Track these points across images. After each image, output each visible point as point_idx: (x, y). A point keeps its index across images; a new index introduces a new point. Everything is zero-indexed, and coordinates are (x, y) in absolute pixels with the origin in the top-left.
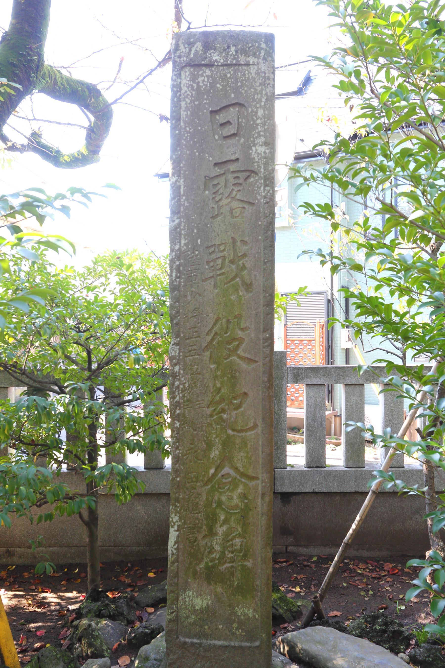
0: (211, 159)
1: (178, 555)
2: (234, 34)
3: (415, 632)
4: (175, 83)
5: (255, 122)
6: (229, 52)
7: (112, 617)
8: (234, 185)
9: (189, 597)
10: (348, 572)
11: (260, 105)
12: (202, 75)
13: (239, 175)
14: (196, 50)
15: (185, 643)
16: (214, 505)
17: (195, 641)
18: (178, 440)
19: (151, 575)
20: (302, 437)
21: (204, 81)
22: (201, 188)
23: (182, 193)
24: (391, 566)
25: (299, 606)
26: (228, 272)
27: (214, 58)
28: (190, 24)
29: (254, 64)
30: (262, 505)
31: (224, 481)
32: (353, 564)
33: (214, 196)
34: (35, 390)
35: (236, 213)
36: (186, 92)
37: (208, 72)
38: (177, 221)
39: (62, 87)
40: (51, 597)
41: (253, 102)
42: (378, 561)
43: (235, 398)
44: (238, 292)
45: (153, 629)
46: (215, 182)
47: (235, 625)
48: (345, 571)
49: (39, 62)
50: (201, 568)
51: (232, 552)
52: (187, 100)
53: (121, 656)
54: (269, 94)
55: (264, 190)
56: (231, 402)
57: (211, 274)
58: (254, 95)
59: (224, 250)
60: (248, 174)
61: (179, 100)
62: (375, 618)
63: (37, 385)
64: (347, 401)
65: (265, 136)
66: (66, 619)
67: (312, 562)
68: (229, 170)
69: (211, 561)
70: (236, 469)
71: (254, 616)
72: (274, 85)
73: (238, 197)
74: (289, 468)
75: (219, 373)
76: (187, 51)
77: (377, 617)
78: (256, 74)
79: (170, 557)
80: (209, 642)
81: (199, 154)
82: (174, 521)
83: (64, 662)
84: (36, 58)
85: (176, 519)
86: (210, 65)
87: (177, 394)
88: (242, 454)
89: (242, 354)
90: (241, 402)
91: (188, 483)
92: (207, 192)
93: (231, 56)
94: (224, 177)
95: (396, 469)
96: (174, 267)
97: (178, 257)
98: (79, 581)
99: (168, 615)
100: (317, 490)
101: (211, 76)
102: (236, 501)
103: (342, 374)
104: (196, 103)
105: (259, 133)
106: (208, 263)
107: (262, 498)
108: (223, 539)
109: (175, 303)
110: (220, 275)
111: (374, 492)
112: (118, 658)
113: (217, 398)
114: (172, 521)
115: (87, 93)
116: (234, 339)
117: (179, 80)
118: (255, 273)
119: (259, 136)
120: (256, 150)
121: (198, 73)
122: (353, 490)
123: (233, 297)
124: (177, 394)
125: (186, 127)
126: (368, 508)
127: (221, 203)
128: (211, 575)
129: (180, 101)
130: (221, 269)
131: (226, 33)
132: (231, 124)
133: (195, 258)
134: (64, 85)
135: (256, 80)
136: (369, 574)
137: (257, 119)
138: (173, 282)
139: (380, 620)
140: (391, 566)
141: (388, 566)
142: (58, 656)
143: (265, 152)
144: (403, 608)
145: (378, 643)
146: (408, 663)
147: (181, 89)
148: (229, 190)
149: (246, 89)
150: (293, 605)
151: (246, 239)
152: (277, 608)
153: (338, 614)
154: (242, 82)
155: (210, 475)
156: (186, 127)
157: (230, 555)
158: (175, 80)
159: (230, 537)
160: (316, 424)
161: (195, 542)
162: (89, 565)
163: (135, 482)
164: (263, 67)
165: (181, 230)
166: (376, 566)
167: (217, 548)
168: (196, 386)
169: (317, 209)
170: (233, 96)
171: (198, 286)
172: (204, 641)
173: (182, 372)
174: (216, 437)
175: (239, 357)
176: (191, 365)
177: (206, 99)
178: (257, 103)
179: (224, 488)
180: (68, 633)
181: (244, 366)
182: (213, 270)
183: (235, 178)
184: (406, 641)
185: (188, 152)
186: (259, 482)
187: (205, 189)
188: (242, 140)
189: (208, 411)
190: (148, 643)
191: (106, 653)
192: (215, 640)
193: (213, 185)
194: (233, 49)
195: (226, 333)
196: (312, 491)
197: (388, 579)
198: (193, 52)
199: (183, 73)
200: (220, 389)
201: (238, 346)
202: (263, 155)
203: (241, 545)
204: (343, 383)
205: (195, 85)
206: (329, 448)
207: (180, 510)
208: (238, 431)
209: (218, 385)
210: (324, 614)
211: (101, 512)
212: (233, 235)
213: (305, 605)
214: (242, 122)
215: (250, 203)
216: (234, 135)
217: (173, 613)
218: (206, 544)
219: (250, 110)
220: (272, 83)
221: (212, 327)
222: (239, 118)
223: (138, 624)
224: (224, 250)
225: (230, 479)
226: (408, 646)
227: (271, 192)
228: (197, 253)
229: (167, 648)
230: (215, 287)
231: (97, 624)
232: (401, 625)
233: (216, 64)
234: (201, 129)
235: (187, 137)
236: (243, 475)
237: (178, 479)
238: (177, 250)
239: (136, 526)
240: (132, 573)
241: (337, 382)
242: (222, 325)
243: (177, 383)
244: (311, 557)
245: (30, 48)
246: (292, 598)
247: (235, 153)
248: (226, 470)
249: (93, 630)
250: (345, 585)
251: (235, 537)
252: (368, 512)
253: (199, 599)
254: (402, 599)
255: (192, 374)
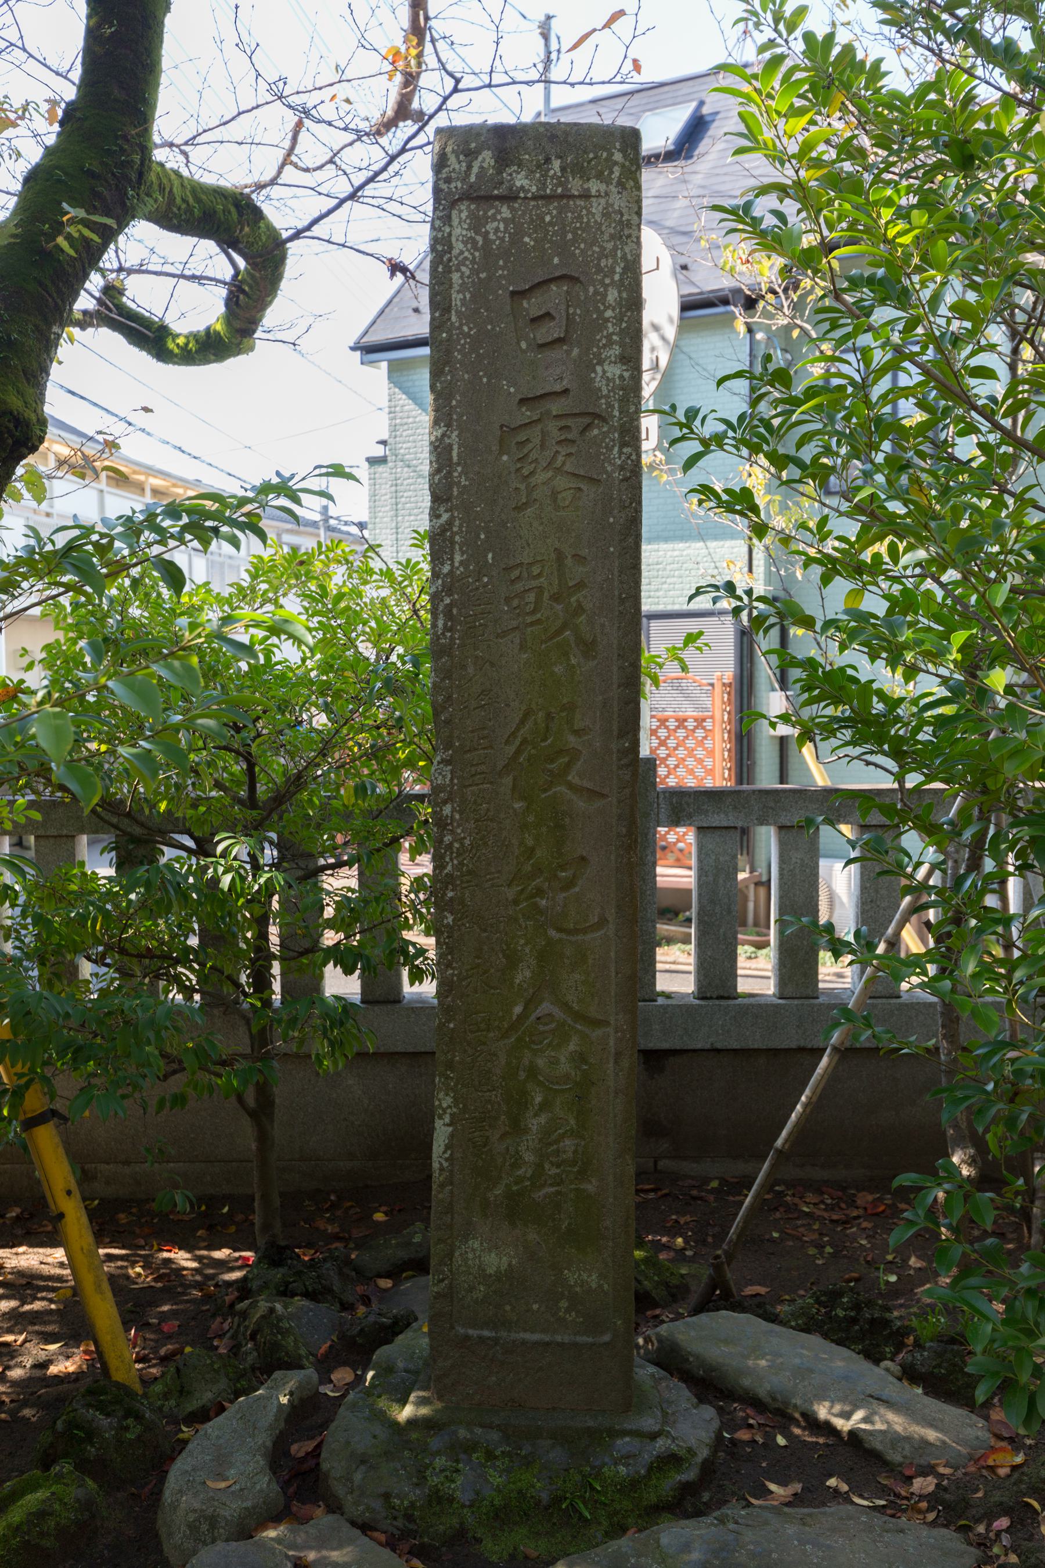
0: (512, 390)
1: (451, 1171)
2: (559, 133)
3: (915, 1323)
4: (440, 235)
5: (601, 313)
6: (549, 170)
7: (311, 1295)
8: (559, 443)
9: (474, 1250)
10: (782, 1209)
11: (612, 279)
12: (494, 218)
13: (569, 422)
14: (481, 167)
15: (467, 1337)
16: (522, 1075)
17: (486, 1333)
18: (451, 950)
19: (379, 1217)
20: (686, 930)
21: (497, 230)
22: (494, 448)
23: (455, 459)
24: (870, 1198)
25: (682, 1276)
26: (548, 618)
27: (518, 184)
28: (458, 81)
29: (599, 196)
30: (617, 1074)
31: (541, 1028)
32: (794, 1195)
33: (519, 465)
34: (133, 842)
35: (564, 499)
36: (462, 252)
37: (505, 212)
38: (445, 517)
39: (184, 206)
40: (182, 1258)
41: (596, 273)
42: (843, 1189)
43: (562, 867)
44: (569, 659)
45: (395, 1317)
46: (522, 437)
47: (564, 1304)
48: (776, 1209)
49: (142, 164)
50: (496, 1196)
51: (558, 1166)
52: (463, 269)
53: (335, 1368)
54: (629, 257)
55: (620, 453)
56: (556, 876)
57: (515, 623)
58: (599, 260)
59: (539, 575)
60: (587, 420)
61: (448, 271)
62: (835, 1295)
63: (137, 831)
64: (783, 860)
65: (622, 345)
66: (219, 1301)
67: (707, 1191)
68: (548, 412)
69: (516, 1183)
70: (566, 1006)
71: (600, 1286)
72: (638, 238)
73: (568, 468)
74: (661, 1001)
75: (531, 819)
76: (464, 169)
77: (840, 1294)
78: (603, 215)
79: (436, 1174)
80: (514, 1336)
81: (489, 381)
82: (445, 1105)
83: (227, 1376)
84: (137, 158)
85: (446, 1102)
86: (510, 197)
87: (447, 859)
88: (577, 976)
89: (576, 781)
90: (574, 876)
91: (471, 1032)
92: (505, 458)
93: (552, 178)
94: (539, 427)
95: (884, 1001)
96: (441, 608)
97: (448, 589)
98: (233, 1229)
99: (434, 1285)
100: (719, 1046)
101: (513, 220)
102: (565, 1067)
103: (772, 804)
104: (483, 275)
105: (609, 337)
106: (508, 600)
107: (616, 1062)
108: (540, 1140)
109: (443, 680)
110: (532, 624)
111: (835, 1049)
112: (330, 1371)
113: (528, 868)
114: (440, 1105)
115: (235, 215)
116: (560, 752)
117: (448, 230)
118: (602, 620)
119: (610, 343)
120: (604, 372)
121: (485, 213)
122: (793, 1045)
123: (558, 669)
124: (447, 859)
125: (461, 325)
126: (824, 1081)
127: (533, 481)
128: (516, 1209)
129: (450, 272)
130: (533, 612)
131: (542, 129)
132: (553, 318)
133: (481, 590)
134: (187, 203)
135: (604, 228)
136: (826, 1215)
137: (606, 308)
138: (438, 639)
139: (845, 1300)
140: (870, 1198)
141: (865, 1198)
142: (216, 1366)
143: (621, 377)
144: (893, 1279)
145: (839, 1343)
146: (900, 1379)
147: (451, 248)
148: (548, 454)
149: (582, 246)
150: (672, 1274)
151: (585, 552)
152: (641, 1278)
153: (762, 1290)
154: (574, 232)
155: (514, 1017)
156: (461, 325)
157: (554, 1171)
158: (440, 230)
159: (554, 1137)
160: (718, 909)
161: (485, 1146)
162: (257, 1197)
163: (355, 1031)
164: (618, 201)
165: (454, 534)
166: (840, 1198)
167: (529, 1157)
168: (486, 844)
169: (725, 497)
170: (556, 260)
171: (489, 646)
172: (503, 1334)
173: (457, 816)
174: (526, 944)
175: (570, 786)
176: (475, 802)
177: (502, 268)
178: (606, 276)
179: (541, 1043)
180: (226, 1326)
181: (580, 804)
182: (519, 615)
183: (561, 429)
184: (898, 1338)
185: (466, 376)
186: (610, 1030)
187: (501, 453)
188: (576, 352)
189: (510, 893)
190: (389, 1342)
191: (305, 1362)
192: (525, 1331)
193: (518, 443)
194: (556, 164)
195: (544, 740)
196: (708, 1046)
197: (865, 1224)
198: (475, 170)
199: (454, 213)
200: (532, 850)
201: (569, 765)
202: (617, 382)
203: (575, 1152)
204: (775, 824)
205: (480, 239)
206: (743, 951)
207: (456, 1085)
208: (568, 932)
209: (530, 842)
210: (734, 1290)
211: (280, 1093)
212: (557, 545)
213: (696, 1274)
214: (574, 313)
215: (592, 480)
216: (560, 341)
217: (443, 1280)
218: (507, 1149)
219: (591, 289)
220: (634, 233)
221: (518, 729)
222: (568, 306)
223: (362, 1310)
224: (539, 575)
225: (553, 1026)
226: (900, 1346)
227: (634, 457)
228: (486, 579)
229: (431, 1346)
230: (522, 647)
231: (285, 1307)
232: (889, 1310)
233: (522, 195)
234: (493, 329)
235: (463, 345)
236: (579, 1016)
237: (452, 1025)
238: (445, 576)
239: (345, 1119)
240: (339, 1213)
241: (762, 822)
242: (536, 723)
243: (448, 839)
244: (707, 1180)
245: (125, 138)
246: (668, 1260)
247: (561, 378)
248: (546, 1007)
249: (280, 1319)
250: (775, 1235)
251: (562, 1137)
252: (824, 1089)
253: (493, 1255)
254: (891, 1262)
255: (477, 821)
